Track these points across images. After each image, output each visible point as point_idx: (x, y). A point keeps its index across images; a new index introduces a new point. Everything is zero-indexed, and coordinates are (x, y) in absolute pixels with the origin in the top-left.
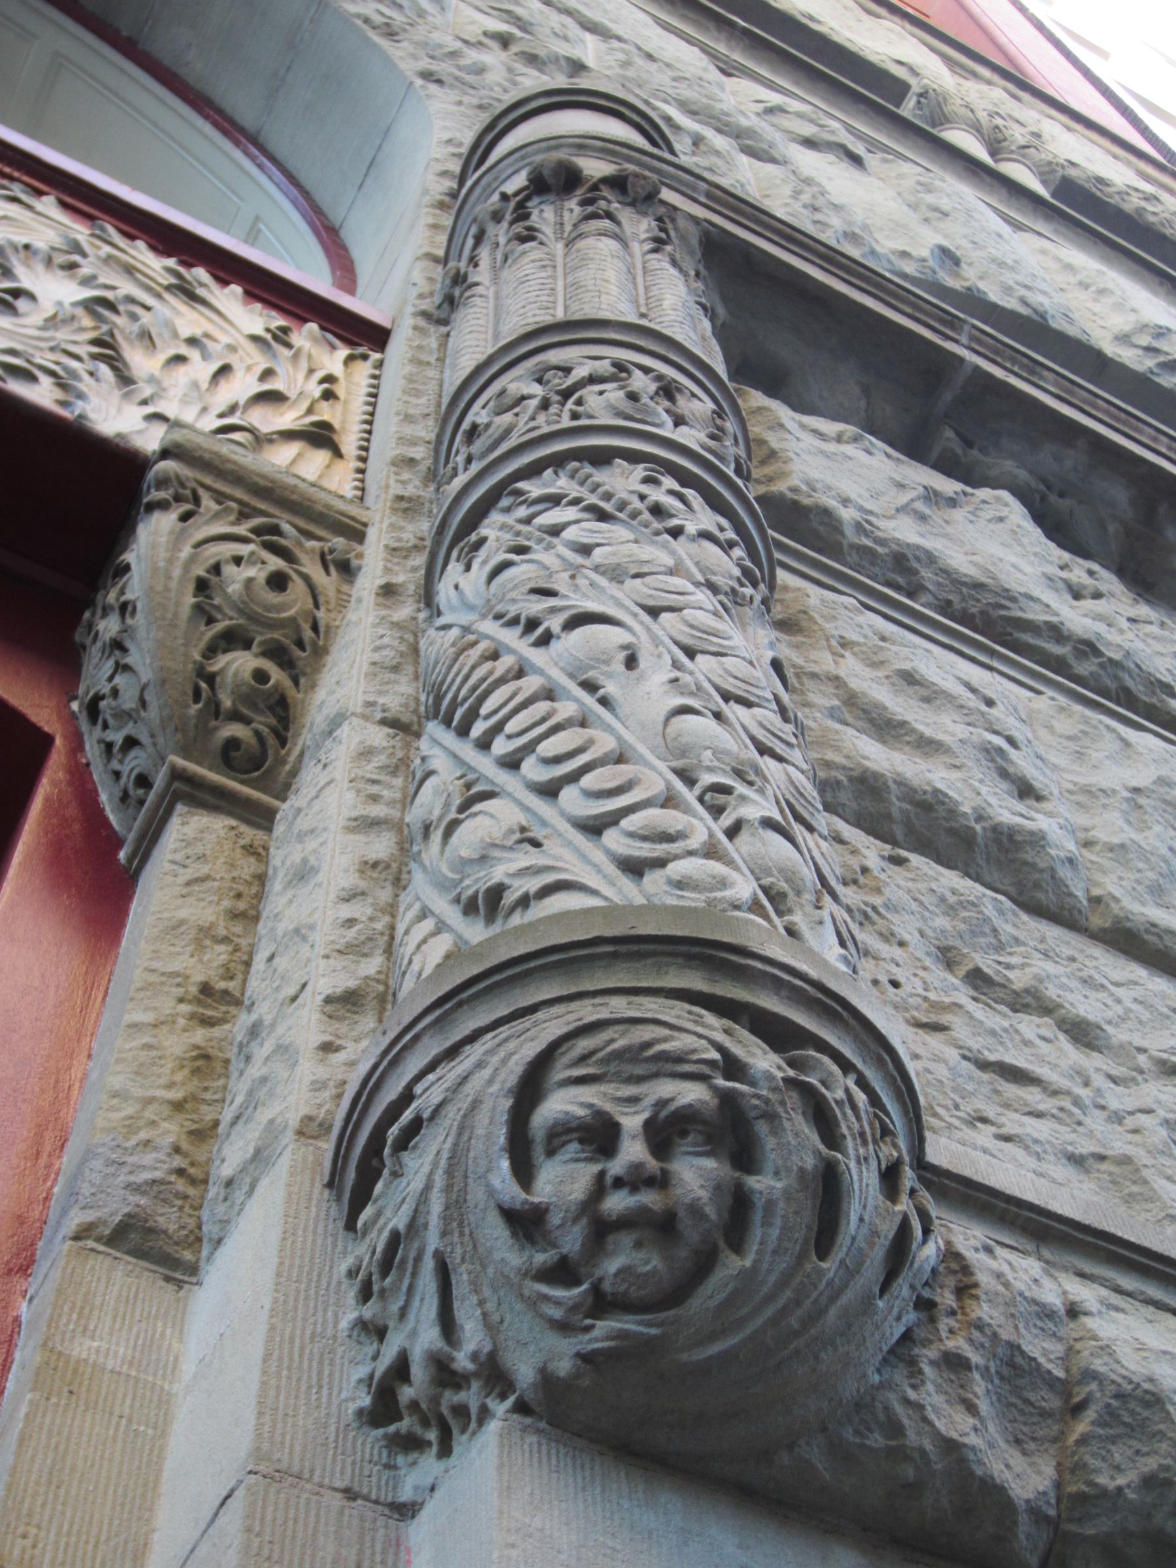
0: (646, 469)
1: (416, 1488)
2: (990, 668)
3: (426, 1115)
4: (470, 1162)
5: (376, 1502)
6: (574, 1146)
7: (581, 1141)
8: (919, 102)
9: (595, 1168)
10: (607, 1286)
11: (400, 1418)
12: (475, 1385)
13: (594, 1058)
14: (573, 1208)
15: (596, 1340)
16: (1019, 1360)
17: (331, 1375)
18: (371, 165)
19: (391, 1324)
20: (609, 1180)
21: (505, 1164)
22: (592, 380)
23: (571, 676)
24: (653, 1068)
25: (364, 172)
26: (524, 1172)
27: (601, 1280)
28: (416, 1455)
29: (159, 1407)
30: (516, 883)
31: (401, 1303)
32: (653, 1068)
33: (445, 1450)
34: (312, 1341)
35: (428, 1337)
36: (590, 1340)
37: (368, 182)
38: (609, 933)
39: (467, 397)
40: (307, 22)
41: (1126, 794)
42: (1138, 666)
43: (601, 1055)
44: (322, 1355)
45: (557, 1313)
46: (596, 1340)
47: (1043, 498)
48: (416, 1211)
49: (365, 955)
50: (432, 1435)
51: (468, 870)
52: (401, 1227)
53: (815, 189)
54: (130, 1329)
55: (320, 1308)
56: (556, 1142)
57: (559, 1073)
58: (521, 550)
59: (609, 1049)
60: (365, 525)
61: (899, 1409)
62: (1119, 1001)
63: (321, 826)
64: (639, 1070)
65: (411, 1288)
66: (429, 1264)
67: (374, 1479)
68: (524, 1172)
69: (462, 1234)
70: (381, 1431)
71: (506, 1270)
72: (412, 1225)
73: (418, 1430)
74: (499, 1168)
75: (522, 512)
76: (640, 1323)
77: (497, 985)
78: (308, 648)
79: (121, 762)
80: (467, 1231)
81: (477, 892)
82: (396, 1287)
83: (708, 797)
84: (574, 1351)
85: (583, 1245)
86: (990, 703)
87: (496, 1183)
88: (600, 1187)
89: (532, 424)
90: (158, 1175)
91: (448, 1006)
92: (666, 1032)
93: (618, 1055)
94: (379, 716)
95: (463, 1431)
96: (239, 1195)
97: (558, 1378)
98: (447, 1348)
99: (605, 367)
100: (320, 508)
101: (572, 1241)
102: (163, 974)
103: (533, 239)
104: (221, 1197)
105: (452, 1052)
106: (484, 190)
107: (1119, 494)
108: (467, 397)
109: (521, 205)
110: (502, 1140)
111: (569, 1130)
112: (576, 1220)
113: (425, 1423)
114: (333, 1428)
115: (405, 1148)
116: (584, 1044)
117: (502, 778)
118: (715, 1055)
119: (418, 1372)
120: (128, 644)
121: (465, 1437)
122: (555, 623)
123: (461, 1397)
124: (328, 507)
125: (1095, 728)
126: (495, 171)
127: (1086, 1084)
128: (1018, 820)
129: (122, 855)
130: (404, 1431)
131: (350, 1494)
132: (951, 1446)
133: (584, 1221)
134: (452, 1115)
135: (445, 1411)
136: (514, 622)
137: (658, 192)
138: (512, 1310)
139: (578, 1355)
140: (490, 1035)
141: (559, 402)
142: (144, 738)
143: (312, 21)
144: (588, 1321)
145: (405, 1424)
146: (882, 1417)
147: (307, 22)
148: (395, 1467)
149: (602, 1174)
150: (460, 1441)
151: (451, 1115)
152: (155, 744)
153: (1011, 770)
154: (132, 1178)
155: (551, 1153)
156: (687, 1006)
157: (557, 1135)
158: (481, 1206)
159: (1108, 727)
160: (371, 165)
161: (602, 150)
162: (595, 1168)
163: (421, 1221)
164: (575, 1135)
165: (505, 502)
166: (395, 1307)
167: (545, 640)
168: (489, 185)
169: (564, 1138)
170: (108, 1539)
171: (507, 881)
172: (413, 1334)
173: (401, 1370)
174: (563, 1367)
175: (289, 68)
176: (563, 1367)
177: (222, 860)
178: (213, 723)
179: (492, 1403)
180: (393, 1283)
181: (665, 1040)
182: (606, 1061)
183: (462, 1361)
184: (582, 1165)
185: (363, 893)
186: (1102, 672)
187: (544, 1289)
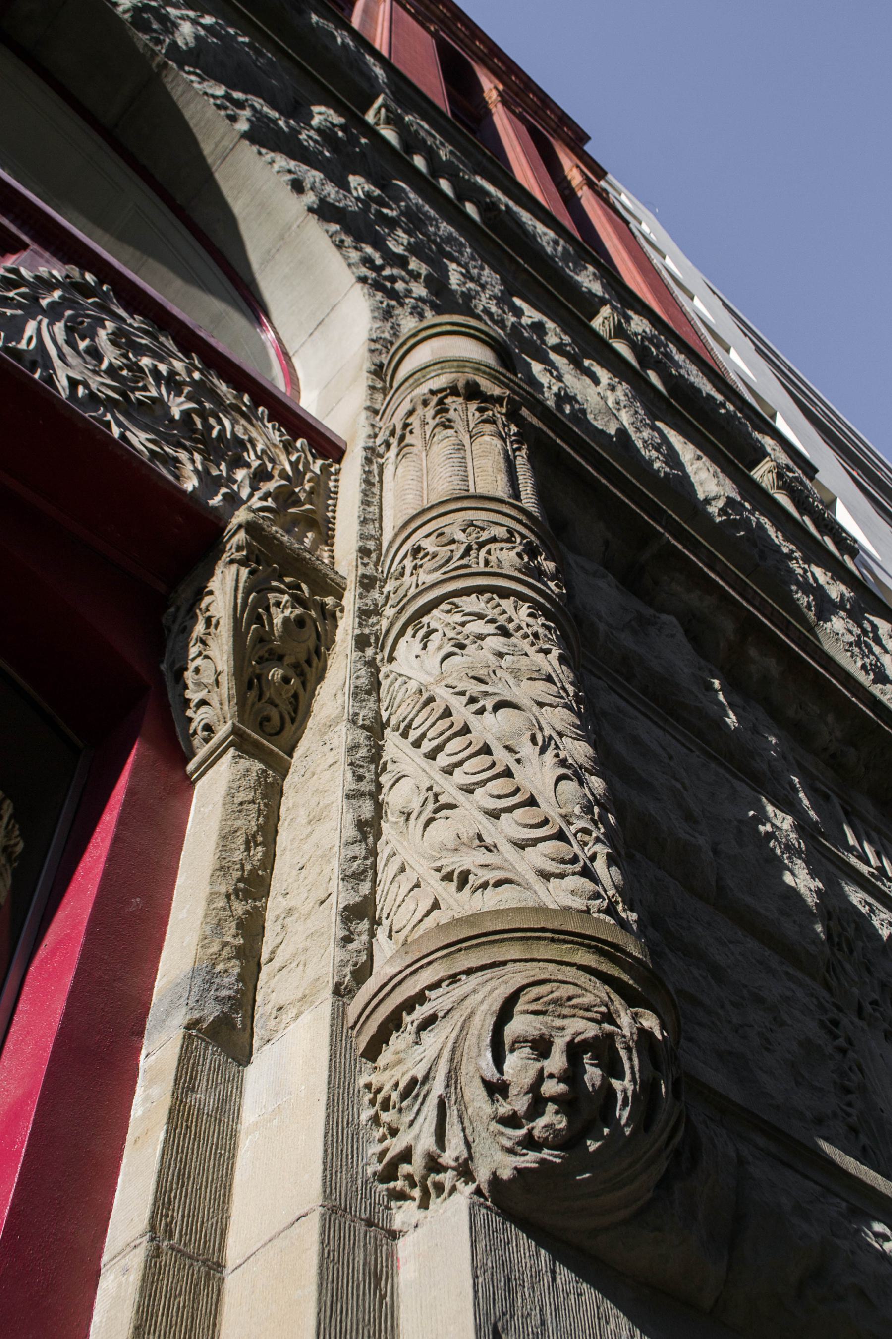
0: (529, 607)
1: (403, 1223)
3: (441, 1014)
4: (466, 1048)
5: (382, 1228)
6: (528, 1050)
7: (531, 1048)
8: (603, 322)
9: (538, 1065)
10: (536, 1133)
11: (396, 1179)
12: (451, 1174)
13: (541, 1001)
14: (526, 1087)
15: (528, 1162)
17: (358, 1148)
18: (320, 323)
19: (402, 1128)
20: (546, 1074)
21: (489, 1055)
22: (494, 540)
23: (498, 739)
24: (573, 1011)
25: (315, 326)
26: (499, 1061)
27: (533, 1128)
28: (402, 1202)
29: (231, 1139)
30: (480, 872)
31: (412, 1118)
32: (573, 1011)
33: (424, 1204)
34: (348, 1126)
35: (426, 1142)
36: (523, 1162)
37: (316, 333)
40: (295, 226)
41: (736, 823)
43: (545, 999)
44: (353, 1134)
45: (509, 1144)
46: (528, 1162)
48: (430, 1069)
49: (362, 881)
50: (416, 1193)
51: (444, 853)
52: (420, 1077)
53: (562, 385)
54: (216, 1087)
55: (350, 1106)
56: (517, 1045)
57: (519, 1007)
58: (462, 646)
59: (550, 997)
60: (344, 589)
62: (733, 954)
63: (332, 789)
64: (566, 1011)
65: (419, 1110)
66: (432, 1102)
67: (380, 1215)
68: (499, 1061)
69: (456, 1088)
70: (385, 1186)
71: (481, 1114)
72: (426, 1078)
73: (407, 1189)
74: (485, 1056)
75: (458, 618)
76: (551, 1155)
79: (195, 712)
80: (459, 1087)
81: (453, 871)
82: (409, 1108)
83: (579, 835)
84: (514, 1165)
85: (528, 1108)
86: (671, 758)
87: (483, 1064)
88: (540, 1078)
89: (464, 562)
90: (231, 993)
91: (453, 949)
92: (580, 992)
93: (556, 1002)
95: (438, 1196)
96: (286, 1017)
97: (502, 1179)
98: (438, 1151)
99: (501, 532)
101: (520, 1104)
103: (451, 427)
104: (273, 1016)
105: (454, 978)
106: (416, 381)
107: (728, 626)
109: (441, 402)
110: (488, 1041)
112: (527, 1093)
113: (413, 1185)
114: (360, 1182)
115: (424, 1029)
116: (535, 992)
117: (460, 798)
119: (418, 1160)
120: (210, 642)
121: (439, 1200)
122: (489, 703)
123: (440, 1177)
126: (424, 372)
127: (722, 1007)
128: (688, 837)
130: (398, 1188)
133: (531, 1095)
134: (457, 1017)
135: (429, 1183)
136: (463, 693)
137: (520, 409)
138: (480, 1136)
139: (516, 1168)
140: (480, 974)
141: (476, 549)
142: (215, 701)
143: (299, 226)
144: (525, 1151)
145: (399, 1184)
147: (295, 226)
148: (390, 1208)
149: (541, 1070)
150: (435, 1203)
151: (456, 1017)
152: (221, 709)
155: (512, 1051)
156: (588, 976)
157: (520, 1042)
158: (470, 1074)
159: (727, 779)
160: (320, 323)
161: (489, 374)
162: (538, 1065)
163: (432, 1075)
164: (529, 1044)
165: (445, 606)
166: (408, 1117)
167: (481, 711)
168: (419, 379)
169: (522, 1044)
170: (208, 1220)
171: (473, 869)
172: (417, 1137)
173: (406, 1156)
174: (506, 1174)
175: (278, 250)
176: (506, 1174)
177: (259, 791)
179: (460, 1185)
180: (408, 1106)
181: (579, 996)
183: (447, 1158)
184: (531, 1062)
187: (502, 1128)
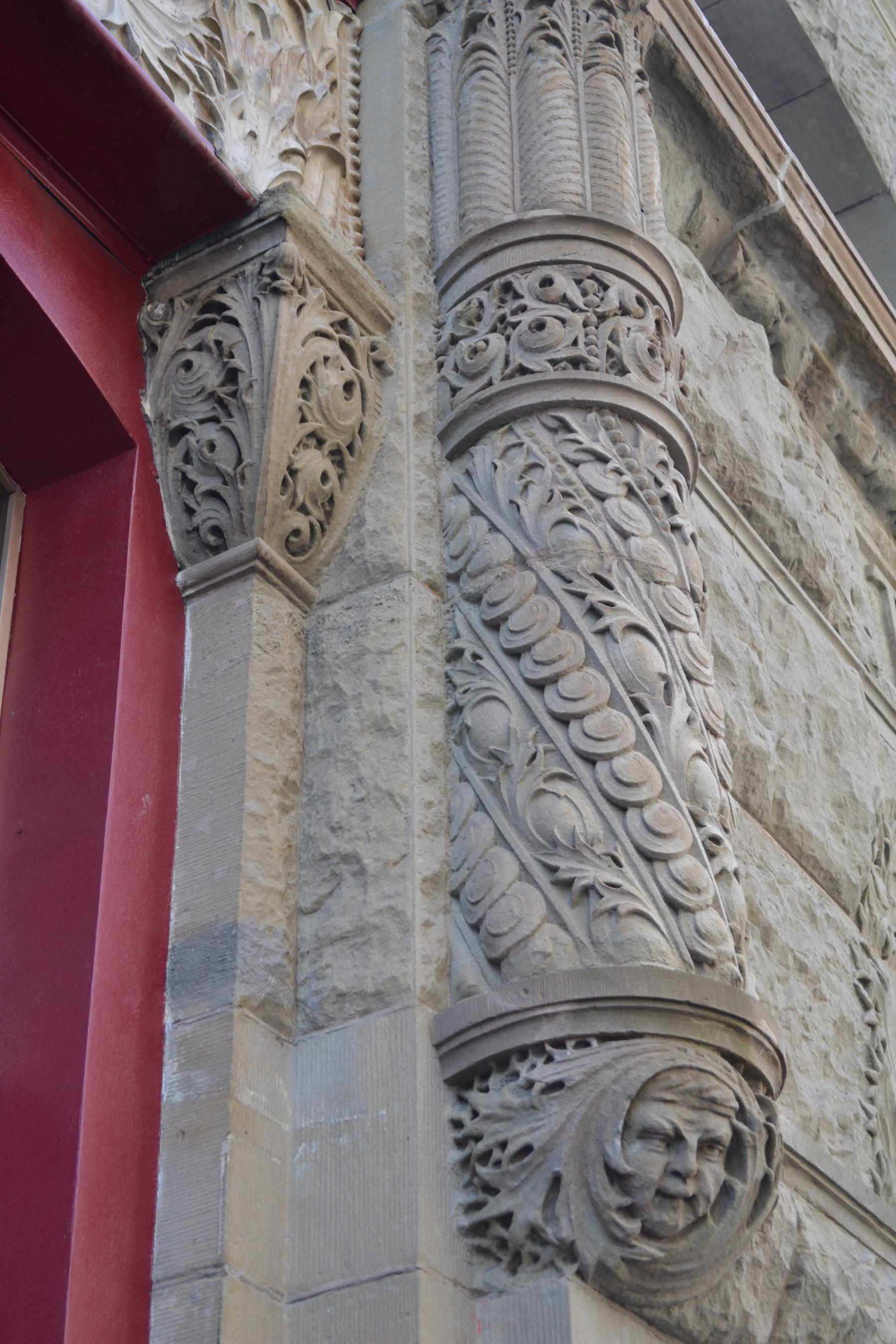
2: (732, 533)
16: (776, 1260)
38: (693, 1000)
39: (503, 240)
42: (813, 543)
47: (776, 322)
61: (730, 1291)
77: (621, 1008)
78: (356, 454)
94: (425, 577)
100: (368, 296)
102: (264, 765)
108: (503, 240)
111: (657, 1133)
116: (675, 1078)
118: (736, 1105)
124: (373, 296)
125: (795, 628)
129: (180, 577)
131: (456, 1283)
132: (746, 1315)
146: (722, 1296)
153: (757, 685)
154: (267, 961)
178: (288, 512)
182: (683, 1093)
185: (435, 778)
186: (792, 545)
